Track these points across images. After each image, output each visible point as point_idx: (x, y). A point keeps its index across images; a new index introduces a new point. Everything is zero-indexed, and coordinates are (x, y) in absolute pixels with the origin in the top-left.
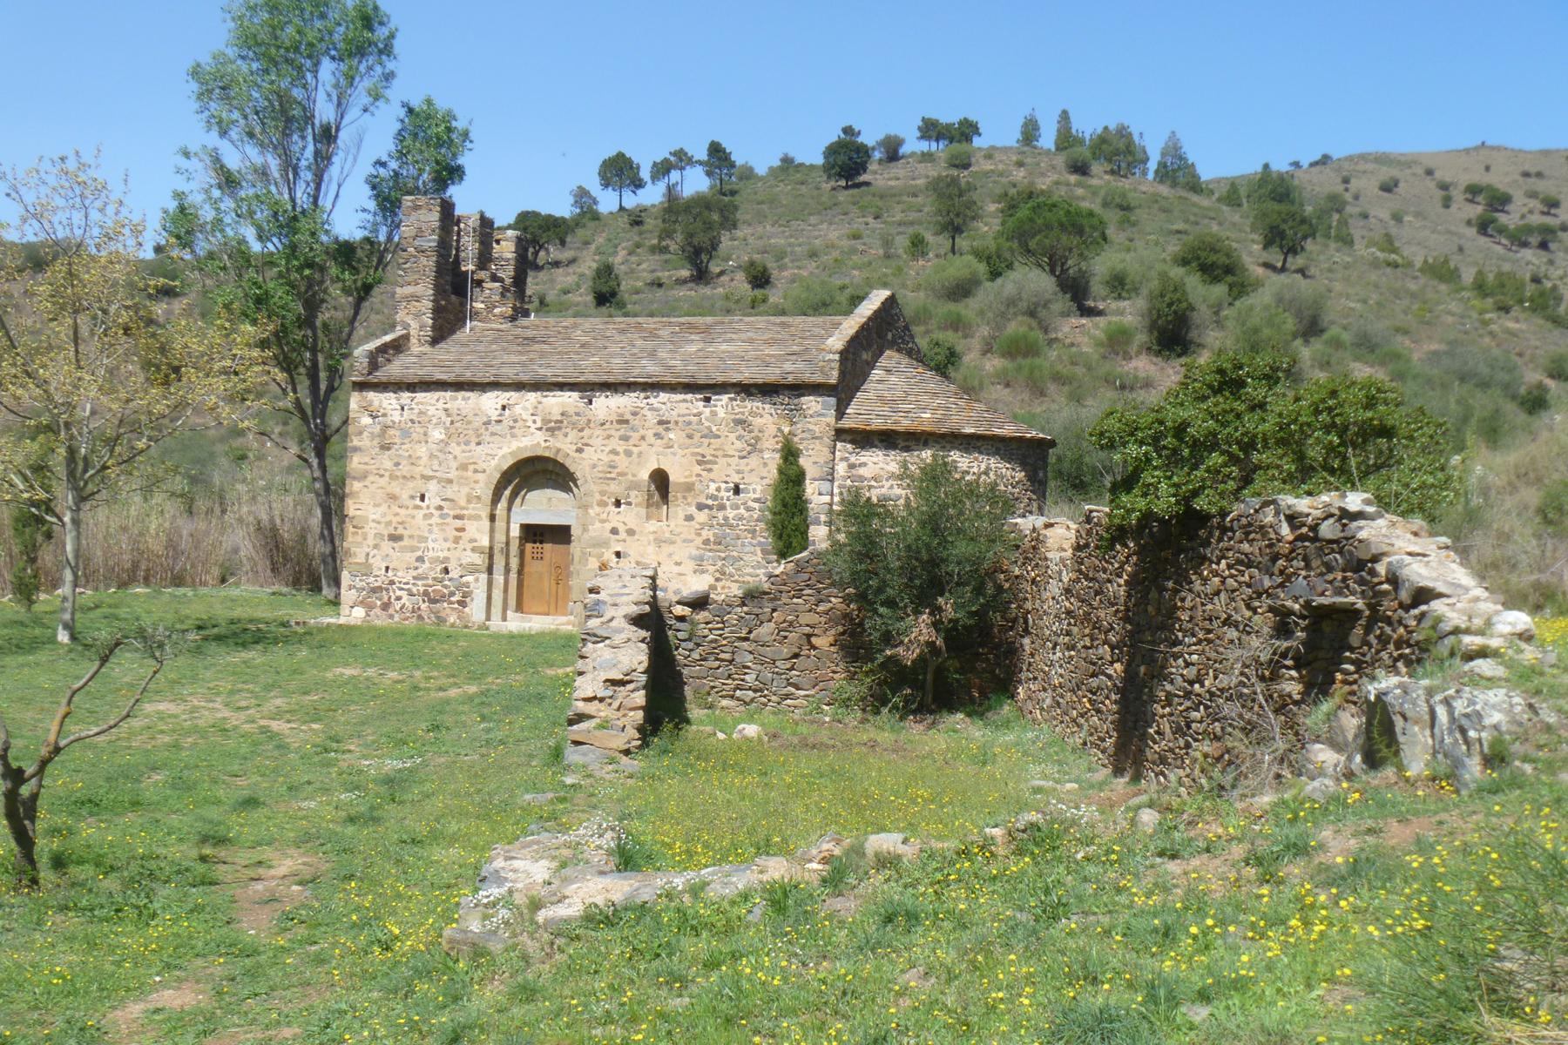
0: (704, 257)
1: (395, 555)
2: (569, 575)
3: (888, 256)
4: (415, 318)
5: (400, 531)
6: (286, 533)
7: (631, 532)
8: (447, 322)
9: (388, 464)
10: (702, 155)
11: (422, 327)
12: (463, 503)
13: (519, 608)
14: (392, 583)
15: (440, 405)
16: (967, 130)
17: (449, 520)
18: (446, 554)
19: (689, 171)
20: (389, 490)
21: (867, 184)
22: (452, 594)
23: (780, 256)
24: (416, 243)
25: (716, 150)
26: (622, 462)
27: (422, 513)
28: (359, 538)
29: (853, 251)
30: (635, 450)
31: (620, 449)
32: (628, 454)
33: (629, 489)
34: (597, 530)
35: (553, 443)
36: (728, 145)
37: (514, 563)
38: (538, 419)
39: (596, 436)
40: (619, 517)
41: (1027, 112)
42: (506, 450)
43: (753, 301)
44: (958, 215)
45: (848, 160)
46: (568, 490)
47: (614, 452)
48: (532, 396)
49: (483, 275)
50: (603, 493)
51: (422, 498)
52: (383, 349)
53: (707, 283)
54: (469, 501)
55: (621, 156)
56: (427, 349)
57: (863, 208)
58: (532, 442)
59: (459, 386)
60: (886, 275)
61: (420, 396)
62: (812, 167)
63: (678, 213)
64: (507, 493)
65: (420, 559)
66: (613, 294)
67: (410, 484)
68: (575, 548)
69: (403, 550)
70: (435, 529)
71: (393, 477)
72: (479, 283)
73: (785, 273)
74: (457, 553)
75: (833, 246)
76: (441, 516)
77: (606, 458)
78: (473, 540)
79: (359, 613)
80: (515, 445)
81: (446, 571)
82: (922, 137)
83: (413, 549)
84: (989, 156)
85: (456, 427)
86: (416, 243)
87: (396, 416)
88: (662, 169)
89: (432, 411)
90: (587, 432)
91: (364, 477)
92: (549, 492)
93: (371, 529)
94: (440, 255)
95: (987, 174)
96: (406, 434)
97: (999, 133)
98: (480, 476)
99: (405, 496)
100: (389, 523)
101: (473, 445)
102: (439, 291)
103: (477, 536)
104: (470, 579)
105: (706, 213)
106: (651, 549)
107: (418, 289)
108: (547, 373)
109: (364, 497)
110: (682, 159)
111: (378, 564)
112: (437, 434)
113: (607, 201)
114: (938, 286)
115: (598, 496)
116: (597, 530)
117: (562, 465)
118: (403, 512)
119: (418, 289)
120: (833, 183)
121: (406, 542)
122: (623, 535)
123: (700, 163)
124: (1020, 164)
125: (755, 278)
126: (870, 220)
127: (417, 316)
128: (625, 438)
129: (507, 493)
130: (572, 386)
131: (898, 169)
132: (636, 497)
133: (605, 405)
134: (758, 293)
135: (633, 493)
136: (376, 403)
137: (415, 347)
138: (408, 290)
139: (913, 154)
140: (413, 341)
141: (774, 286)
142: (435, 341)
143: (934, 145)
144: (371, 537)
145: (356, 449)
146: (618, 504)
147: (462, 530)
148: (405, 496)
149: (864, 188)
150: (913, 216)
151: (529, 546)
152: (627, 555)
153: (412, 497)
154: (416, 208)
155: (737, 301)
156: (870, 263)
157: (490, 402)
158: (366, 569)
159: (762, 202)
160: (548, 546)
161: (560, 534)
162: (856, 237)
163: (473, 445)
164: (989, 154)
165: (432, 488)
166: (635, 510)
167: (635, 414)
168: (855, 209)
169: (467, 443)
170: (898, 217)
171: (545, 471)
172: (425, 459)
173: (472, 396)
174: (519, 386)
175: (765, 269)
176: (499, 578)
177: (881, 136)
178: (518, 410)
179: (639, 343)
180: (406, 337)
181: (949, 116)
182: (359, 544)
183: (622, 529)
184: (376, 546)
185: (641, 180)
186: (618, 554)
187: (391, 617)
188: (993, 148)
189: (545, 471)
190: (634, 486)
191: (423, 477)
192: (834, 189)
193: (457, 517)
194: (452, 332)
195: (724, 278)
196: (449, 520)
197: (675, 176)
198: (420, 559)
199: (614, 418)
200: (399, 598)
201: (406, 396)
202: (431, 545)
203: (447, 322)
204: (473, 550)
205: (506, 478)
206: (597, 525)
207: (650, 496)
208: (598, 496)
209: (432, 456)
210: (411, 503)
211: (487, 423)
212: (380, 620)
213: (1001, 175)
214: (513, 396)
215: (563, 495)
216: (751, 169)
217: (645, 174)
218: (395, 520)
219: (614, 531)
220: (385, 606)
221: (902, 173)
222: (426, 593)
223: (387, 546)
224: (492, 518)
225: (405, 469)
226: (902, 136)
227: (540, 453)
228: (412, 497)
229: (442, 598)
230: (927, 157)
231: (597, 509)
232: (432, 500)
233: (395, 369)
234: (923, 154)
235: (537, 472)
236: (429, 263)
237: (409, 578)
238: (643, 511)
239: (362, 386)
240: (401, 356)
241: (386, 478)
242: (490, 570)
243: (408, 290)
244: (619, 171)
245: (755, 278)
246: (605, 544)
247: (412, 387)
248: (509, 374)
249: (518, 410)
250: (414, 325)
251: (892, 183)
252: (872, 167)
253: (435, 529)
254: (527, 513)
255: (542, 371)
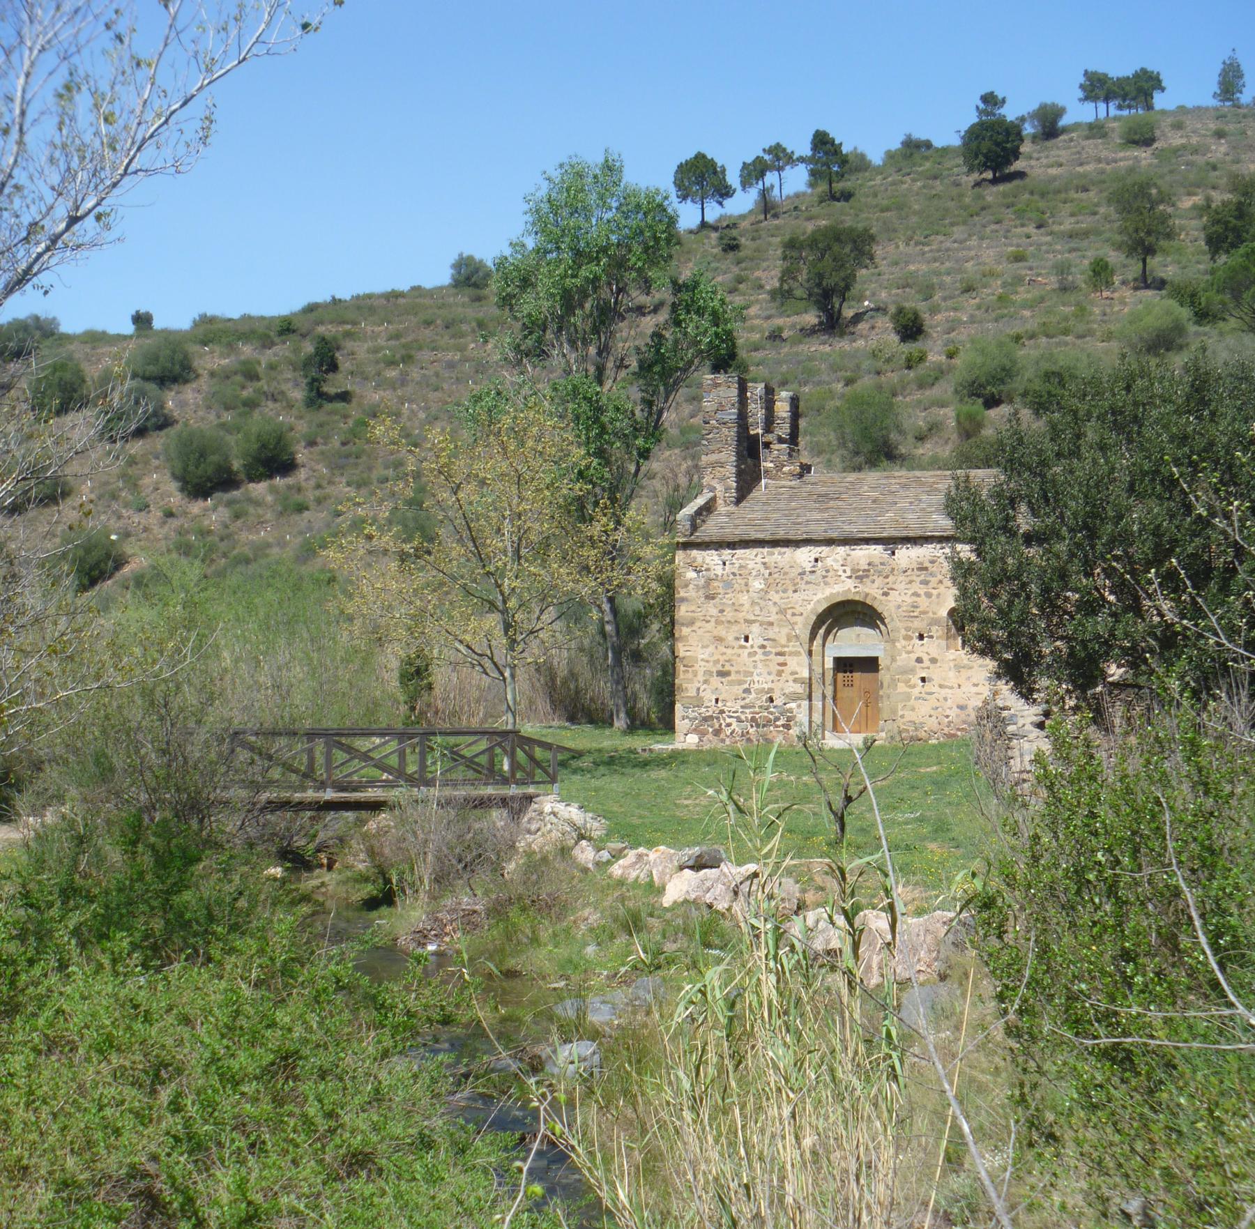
0: (836, 301)
1: (723, 688)
2: (878, 698)
3: (1064, 289)
4: (719, 479)
5: (727, 668)
6: (562, 672)
7: (934, 661)
8: (747, 480)
9: (714, 612)
10: (802, 147)
11: (727, 489)
12: (783, 641)
13: (835, 728)
14: (722, 712)
15: (759, 559)
16: (1143, 87)
17: (772, 656)
18: (770, 685)
19: (788, 172)
20: (716, 633)
21: (1021, 175)
22: (777, 719)
23: (927, 292)
24: (718, 416)
25: (822, 141)
26: (923, 602)
27: (746, 651)
28: (690, 675)
29: (1019, 280)
30: (935, 592)
31: (922, 592)
32: (929, 595)
33: (930, 624)
34: (904, 659)
35: (861, 588)
36: (837, 135)
37: (829, 691)
38: (848, 569)
39: (900, 582)
40: (920, 648)
41: (1225, 55)
42: (820, 596)
43: (909, 360)
44: (1149, 233)
45: (994, 147)
46: (874, 626)
47: (916, 594)
48: (842, 550)
49: (770, 437)
50: (908, 629)
51: (747, 639)
52: (699, 512)
53: (842, 334)
54: (789, 640)
55: (700, 157)
56: (732, 508)
57: (1020, 214)
58: (844, 588)
59: (775, 543)
60: (1066, 319)
61: (740, 552)
62: (945, 151)
63: (801, 248)
64: (822, 631)
65: (747, 691)
66: (733, 355)
67: (735, 628)
68: (884, 675)
69: (731, 683)
70: (760, 665)
71: (718, 622)
72: (767, 445)
73: (939, 317)
74: (780, 685)
75: (992, 274)
76: (765, 654)
77: (909, 600)
78: (793, 673)
79: (693, 739)
80: (828, 591)
81: (771, 700)
82: (1086, 98)
83: (740, 683)
84: (1178, 126)
85: (774, 578)
86: (718, 416)
87: (719, 570)
88: (754, 171)
89: (751, 565)
90: (891, 579)
91: (692, 623)
92: (858, 629)
93: (701, 667)
94: (740, 426)
95: (1176, 151)
96: (728, 585)
97: (1187, 89)
98: (799, 619)
99: (730, 638)
100: (717, 662)
101: (790, 593)
102: (740, 456)
103: (798, 669)
104: (793, 705)
105: (836, 248)
106: (952, 674)
107: (722, 456)
108: (853, 530)
109: (693, 640)
110: (779, 157)
111: (709, 697)
112: (757, 585)
113: (688, 216)
114: (1135, 340)
115: (903, 632)
116: (904, 659)
117: (871, 607)
118: (729, 651)
119: (722, 456)
120: (975, 176)
121: (733, 677)
122: (927, 663)
123: (802, 160)
124: (1220, 134)
125: (905, 327)
126: (1031, 229)
127: (723, 479)
128: (925, 583)
129: (822, 631)
130: (876, 541)
131: (1059, 150)
132: (936, 631)
133: (907, 555)
134: (907, 348)
135: (934, 628)
136: (699, 560)
137: (721, 508)
138: (713, 457)
139: (1076, 126)
140: (720, 501)
141: (927, 336)
142: (739, 501)
143: (1102, 106)
144: (700, 674)
145: (683, 600)
146: (921, 637)
147: (785, 664)
148: (730, 638)
149: (1016, 182)
150: (1086, 223)
151: (840, 675)
152: (931, 680)
153: (737, 639)
154: (716, 385)
155: (888, 361)
156: (1042, 299)
157: (804, 556)
158: (698, 702)
159: (887, 209)
160: (857, 675)
161: (870, 664)
162: (1019, 258)
163: (790, 593)
164: (1180, 118)
165: (755, 630)
166: (936, 642)
167: (932, 562)
168: (1009, 214)
169: (785, 591)
170: (1068, 225)
171: (853, 612)
172: (747, 606)
173: (788, 551)
174: (830, 542)
175: (916, 316)
176: (818, 704)
177: (1033, 106)
178: (829, 562)
179: (924, 497)
180: (713, 499)
181: (1120, 68)
182: (690, 681)
183: (926, 658)
184: (706, 682)
185: (728, 187)
186: (923, 680)
187: (723, 741)
188: (1182, 109)
189: (853, 612)
190: (935, 622)
191: (746, 621)
192: (978, 184)
193: (778, 654)
194: (750, 491)
195: (862, 326)
196: (772, 656)
197: (771, 178)
198: (747, 691)
199: (915, 566)
200: (729, 725)
201: (727, 553)
202: (756, 678)
203: (747, 480)
204: (795, 681)
205: (821, 620)
206: (904, 655)
207: (949, 630)
208: (903, 632)
209: (753, 603)
210: (736, 644)
211: (803, 573)
212: (710, 743)
213: (1195, 151)
214: (825, 550)
215: (871, 631)
216: (862, 157)
217: (733, 179)
218: (722, 658)
219: (919, 660)
220: (717, 732)
221: (1064, 155)
222: (753, 719)
223: (715, 681)
224: (810, 653)
225: (729, 614)
226: (1061, 103)
227: (850, 597)
228: (737, 639)
229: (768, 723)
230: (1096, 130)
231: (904, 642)
232: (756, 640)
233: (711, 528)
234: (1091, 126)
235: (847, 613)
236: (730, 433)
237: (738, 707)
238: (943, 643)
239: (686, 546)
240: (712, 517)
241: (713, 623)
242: (810, 698)
243: (713, 457)
244: (700, 176)
245: (905, 327)
246: (912, 671)
247: (732, 545)
248: (818, 531)
249: (829, 562)
250: (720, 488)
251: (1053, 171)
252: (1025, 148)
253: (760, 665)
254: (839, 647)
255: (847, 528)
